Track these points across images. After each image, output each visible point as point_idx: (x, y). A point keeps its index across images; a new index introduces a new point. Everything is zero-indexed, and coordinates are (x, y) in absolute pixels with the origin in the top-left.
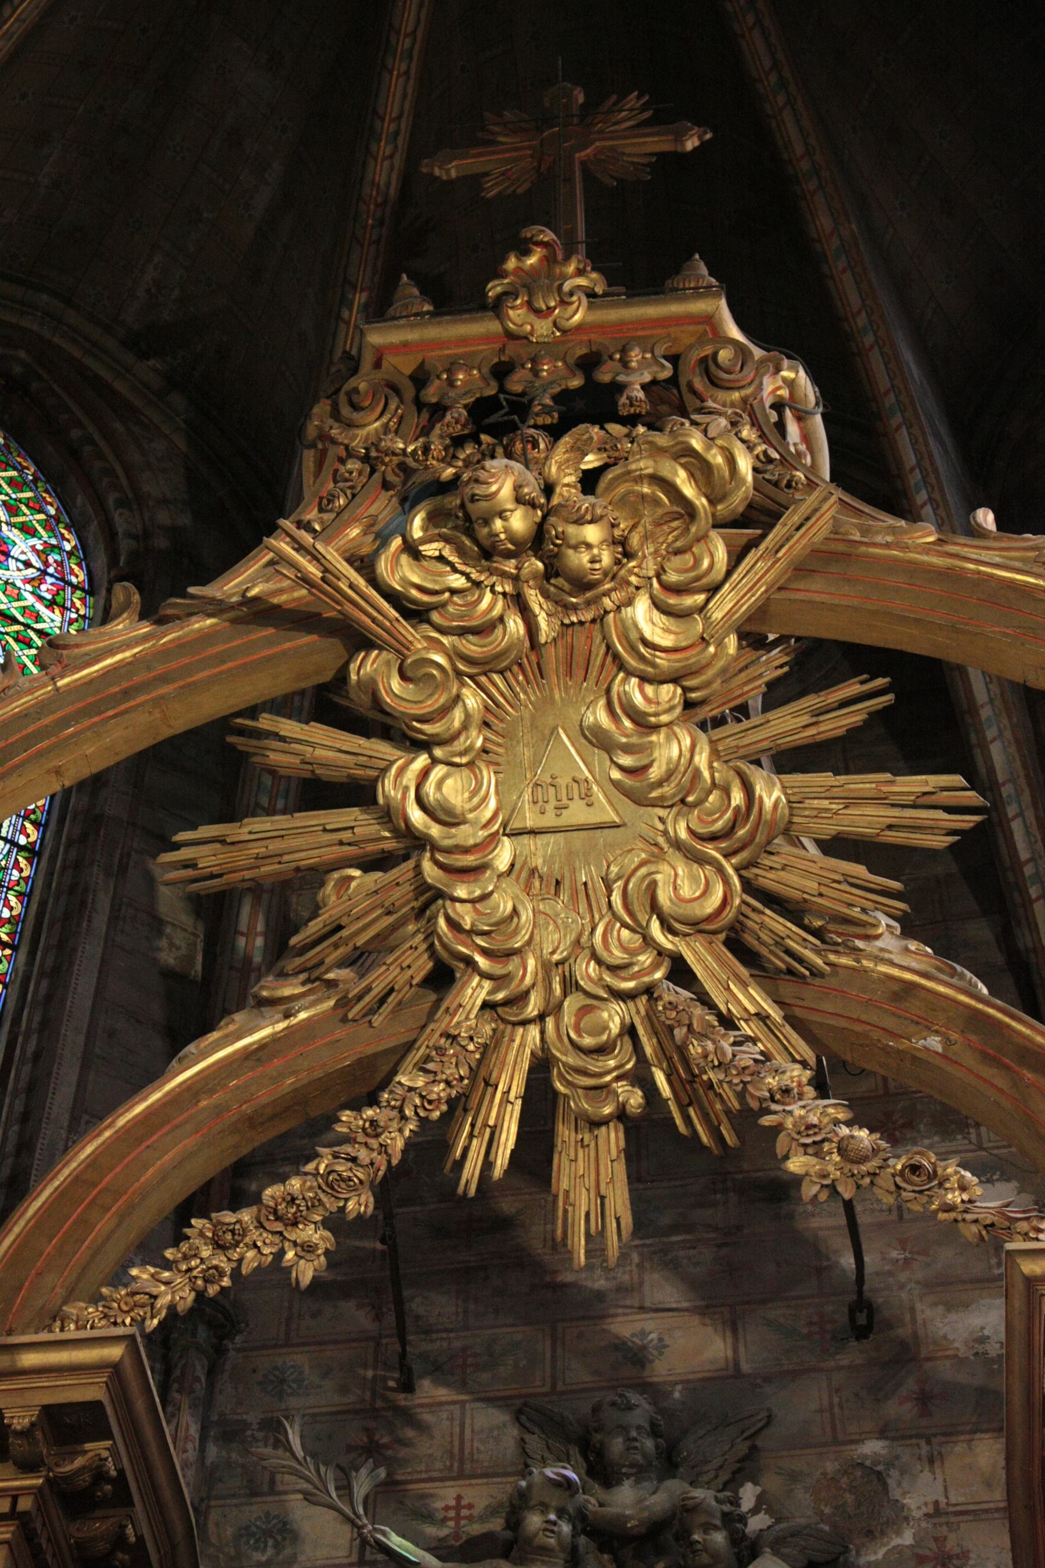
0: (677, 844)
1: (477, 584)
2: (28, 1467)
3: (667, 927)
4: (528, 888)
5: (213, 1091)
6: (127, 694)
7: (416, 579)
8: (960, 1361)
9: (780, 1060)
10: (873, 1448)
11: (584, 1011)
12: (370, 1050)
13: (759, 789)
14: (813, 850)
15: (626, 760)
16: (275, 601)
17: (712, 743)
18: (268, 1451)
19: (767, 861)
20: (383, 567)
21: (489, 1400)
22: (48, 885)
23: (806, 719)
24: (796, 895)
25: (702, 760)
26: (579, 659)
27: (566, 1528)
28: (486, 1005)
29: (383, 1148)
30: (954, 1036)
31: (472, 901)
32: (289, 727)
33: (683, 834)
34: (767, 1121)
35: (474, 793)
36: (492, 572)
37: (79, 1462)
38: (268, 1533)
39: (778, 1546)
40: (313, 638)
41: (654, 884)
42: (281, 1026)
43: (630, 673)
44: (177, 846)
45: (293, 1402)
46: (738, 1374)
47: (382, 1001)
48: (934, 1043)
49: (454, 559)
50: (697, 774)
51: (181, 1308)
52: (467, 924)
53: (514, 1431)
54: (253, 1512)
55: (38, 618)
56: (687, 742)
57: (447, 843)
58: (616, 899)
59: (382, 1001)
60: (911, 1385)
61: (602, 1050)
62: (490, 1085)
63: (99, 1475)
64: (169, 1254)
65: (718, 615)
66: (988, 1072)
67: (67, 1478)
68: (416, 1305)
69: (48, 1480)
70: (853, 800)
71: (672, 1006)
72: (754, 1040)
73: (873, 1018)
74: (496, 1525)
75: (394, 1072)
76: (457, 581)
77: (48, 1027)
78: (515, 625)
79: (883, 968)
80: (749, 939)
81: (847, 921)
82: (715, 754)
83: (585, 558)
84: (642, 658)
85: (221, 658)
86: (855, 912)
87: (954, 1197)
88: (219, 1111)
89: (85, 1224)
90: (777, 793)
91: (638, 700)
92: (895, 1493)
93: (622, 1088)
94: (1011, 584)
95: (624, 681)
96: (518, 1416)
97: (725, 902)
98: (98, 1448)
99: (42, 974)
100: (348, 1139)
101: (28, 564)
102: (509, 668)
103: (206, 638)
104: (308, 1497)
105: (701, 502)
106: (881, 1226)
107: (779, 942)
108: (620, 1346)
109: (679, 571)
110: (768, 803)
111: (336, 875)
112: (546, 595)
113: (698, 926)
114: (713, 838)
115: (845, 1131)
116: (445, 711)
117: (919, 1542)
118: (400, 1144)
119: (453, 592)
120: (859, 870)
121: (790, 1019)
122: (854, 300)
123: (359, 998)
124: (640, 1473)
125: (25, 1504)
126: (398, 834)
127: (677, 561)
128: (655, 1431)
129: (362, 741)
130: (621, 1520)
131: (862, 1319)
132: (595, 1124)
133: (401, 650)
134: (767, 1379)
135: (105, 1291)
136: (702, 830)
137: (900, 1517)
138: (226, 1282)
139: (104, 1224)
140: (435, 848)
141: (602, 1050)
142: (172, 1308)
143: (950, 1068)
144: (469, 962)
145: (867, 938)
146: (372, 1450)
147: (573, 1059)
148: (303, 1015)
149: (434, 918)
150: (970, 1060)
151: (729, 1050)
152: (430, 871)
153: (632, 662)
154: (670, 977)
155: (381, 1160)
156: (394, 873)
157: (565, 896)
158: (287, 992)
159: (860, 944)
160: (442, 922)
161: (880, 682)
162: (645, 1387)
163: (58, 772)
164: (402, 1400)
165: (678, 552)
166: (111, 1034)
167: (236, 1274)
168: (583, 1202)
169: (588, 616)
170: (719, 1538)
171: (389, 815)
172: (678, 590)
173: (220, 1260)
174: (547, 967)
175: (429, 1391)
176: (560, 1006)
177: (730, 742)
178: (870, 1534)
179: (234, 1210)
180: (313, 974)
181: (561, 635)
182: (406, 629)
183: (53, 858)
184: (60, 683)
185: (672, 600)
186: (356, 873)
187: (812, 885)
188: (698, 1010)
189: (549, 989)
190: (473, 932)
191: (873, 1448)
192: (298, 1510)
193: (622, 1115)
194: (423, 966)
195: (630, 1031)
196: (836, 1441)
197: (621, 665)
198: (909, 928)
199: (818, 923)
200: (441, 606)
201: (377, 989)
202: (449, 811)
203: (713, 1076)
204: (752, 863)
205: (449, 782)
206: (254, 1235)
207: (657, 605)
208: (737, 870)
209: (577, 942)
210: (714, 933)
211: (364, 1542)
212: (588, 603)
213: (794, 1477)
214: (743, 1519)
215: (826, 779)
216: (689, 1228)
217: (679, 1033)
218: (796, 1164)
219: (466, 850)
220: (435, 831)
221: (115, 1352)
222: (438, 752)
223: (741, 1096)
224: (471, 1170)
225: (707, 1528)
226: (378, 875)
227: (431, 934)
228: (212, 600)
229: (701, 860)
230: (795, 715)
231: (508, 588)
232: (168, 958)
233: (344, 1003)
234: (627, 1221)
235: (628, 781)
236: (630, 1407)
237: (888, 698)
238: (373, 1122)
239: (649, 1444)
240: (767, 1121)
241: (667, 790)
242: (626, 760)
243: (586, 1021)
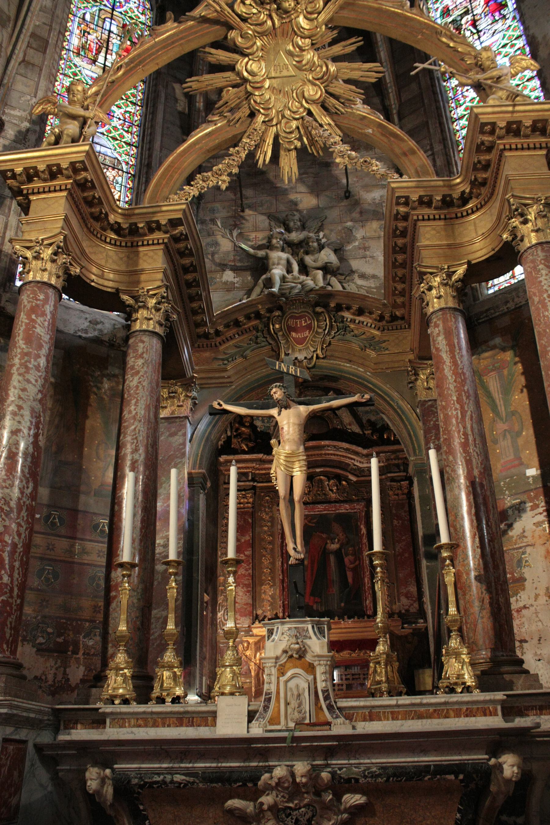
0: (309, 81)
1: (260, 12)
2: (166, 232)
3: (307, 102)
4: (273, 92)
5: (199, 144)
6: (173, 43)
7: (244, 10)
8: (369, 204)
9: (334, 135)
10: (349, 224)
11: (287, 123)
12: (236, 133)
13: (330, 67)
14: (341, 82)
15: (297, 59)
16: (208, 16)
17: (318, 54)
18: (212, 226)
19: (331, 85)
20: (236, 7)
21: (262, 214)
22: (149, 90)
23: (341, 48)
24: (338, 94)
25: (316, 59)
26: (285, 32)
27: (281, 242)
28: (263, 122)
29: (240, 157)
30: (375, 129)
31: (260, 96)
32: (213, 51)
33: (311, 78)
34: (331, 150)
35: (260, 68)
36: (263, 8)
37: (177, 231)
38: (213, 244)
39: (328, 245)
40: (218, 27)
41: (303, 92)
42: (214, 127)
43: (298, 36)
44: (187, 82)
45: (217, 215)
46: (319, 207)
47: (238, 121)
48: (370, 131)
49: (254, 5)
50: (314, 63)
51: (196, 196)
52: (258, 101)
53: (268, 221)
54: (209, 240)
55: (139, 18)
56: (312, 54)
57: (253, 81)
58: (294, 95)
59: (238, 121)
60: (358, 210)
61: (291, 133)
62: (265, 141)
63: (182, 234)
64: (192, 183)
65: (320, 20)
66: (383, 138)
67: (175, 235)
68: (244, 192)
70: (352, 70)
71: (308, 122)
72: (327, 130)
73: (356, 124)
74: (264, 242)
75: (241, 138)
76: (255, 11)
77: (152, 127)
78: (269, 23)
79: (358, 112)
80: (326, 105)
81: (350, 100)
82: (319, 57)
83: (287, 4)
84: (301, 32)
85: (196, 32)
86: (352, 98)
87: (375, 168)
88: (201, 148)
89: (172, 176)
90: (334, 68)
91: (300, 43)
92: (354, 234)
93: (296, 141)
94: (394, 12)
96: (268, 217)
97: (321, 96)
98: (181, 228)
99: (150, 113)
100: (231, 155)
101: (135, 3)
103: (191, 27)
104: (223, 237)
106: (352, 173)
107: (334, 105)
108: (291, 201)
109: (311, 8)
110: (332, 70)
111: (226, 89)
112: (277, 15)
113: (314, 102)
114: (318, 79)
115: (349, 152)
116: (252, 46)
117: (360, 244)
118: (244, 156)
119: (254, 14)
120: (353, 88)
121: (336, 125)
123: (233, 120)
124: (297, 230)
125: (166, 241)
126: (241, 79)
127: (310, 5)
128: (300, 221)
129: (231, 54)
130: (293, 241)
131: (347, 195)
132: (289, 150)
133: (241, 30)
134: (326, 208)
135: (178, 192)
136: (316, 77)
137: (356, 239)
138: (206, 189)
139: (176, 176)
140: (250, 82)
141: (291, 133)
142: (194, 196)
143: (374, 137)
144: (259, 111)
145: (355, 104)
146: (235, 226)
147: (284, 135)
148: (219, 125)
149: (250, 100)
150: (378, 135)
151: (322, 133)
152: (249, 88)
153: (299, 33)
154: (308, 114)
155: (240, 160)
156: (240, 88)
157: (282, 94)
158: (215, 119)
159: (353, 106)
160: (252, 101)
161: (360, 38)
162: (297, 211)
163: (157, 64)
164: (241, 214)
165: (311, 3)
166: (168, 128)
167: (208, 188)
168: (287, 169)
169: (288, 20)
170: (315, 244)
171: (239, 74)
173: (204, 184)
174: (278, 112)
175: (248, 212)
176: (281, 122)
177: (323, 54)
178: (348, 243)
179: (207, 172)
180: (221, 114)
181: (281, 26)
182: (242, 24)
183: (149, 83)
184: (157, 40)
185: (309, 16)
186: (231, 89)
187: (342, 91)
188: (314, 123)
189: (278, 118)
190: (260, 103)
191: (349, 224)
192: (220, 239)
193: (296, 148)
194: (248, 112)
195: (298, 128)
196: (341, 222)
197: (296, 34)
198: (365, 102)
199: (343, 101)
200: (251, 18)
201: (237, 118)
202: (254, 73)
203: (317, 138)
204: (327, 86)
205: (253, 65)
206: (212, 178)
207: (305, 17)
208: (324, 87)
209: (285, 106)
211: (235, 245)
212: (288, 17)
213: (331, 231)
214: (321, 240)
215: (346, 64)
216: (307, 173)
217: (310, 128)
218: (338, 160)
219: (258, 83)
220: (250, 78)
221: (184, 207)
222: (250, 57)
223: (324, 144)
224: (261, 162)
225: (313, 242)
226: (236, 89)
227: (249, 104)
228: (192, 17)
229: (315, 85)
230: (339, 47)
231: (268, 13)
232: (180, 109)
233: (229, 121)
234: (297, 173)
235: (298, 65)
236: (294, 215)
237: (362, 43)
238: (238, 151)
239: (299, 223)
240: (331, 150)
241: (307, 67)
242: (297, 59)
243: (288, 125)
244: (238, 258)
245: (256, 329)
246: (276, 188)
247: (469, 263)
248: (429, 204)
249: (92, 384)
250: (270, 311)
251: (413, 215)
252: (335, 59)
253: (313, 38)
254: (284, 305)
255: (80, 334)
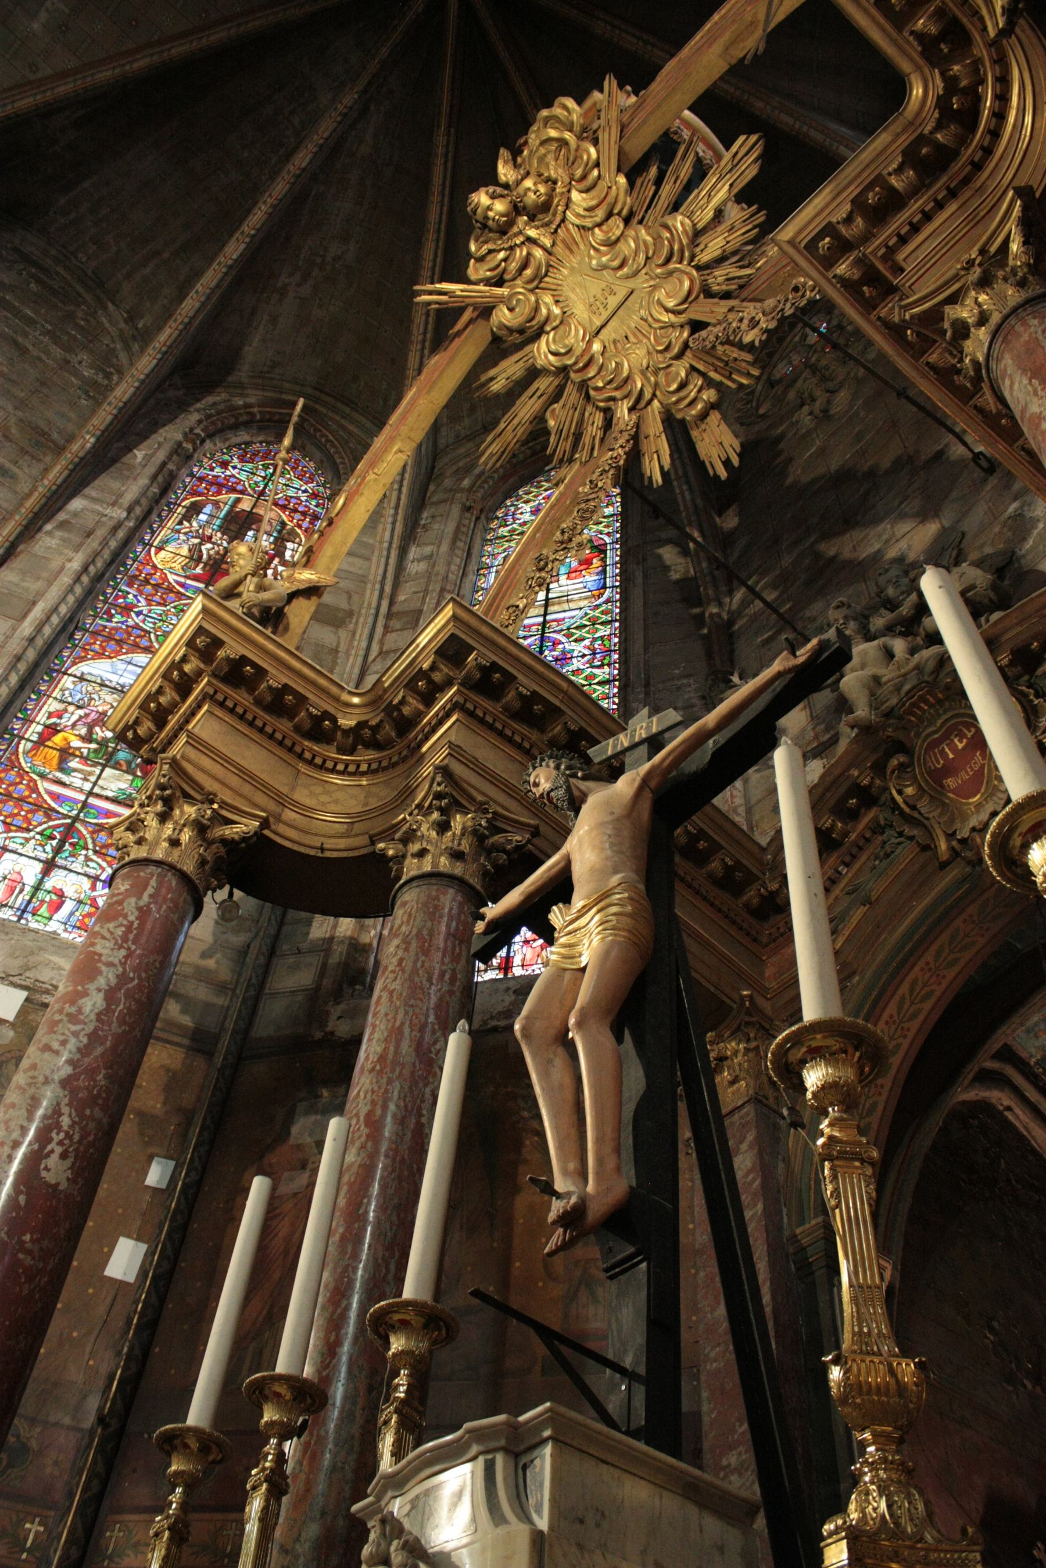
69: (460, 684)
95: (593, 234)
97: (692, 281)
102: (547, 271)
105: (567, 135)
119: (505, 260)
122: (790, 120)
144: (613, 399)
172: (584, 177)
204: (692, 258)
210: (697, 297)
229: (670, 274)
244: (822, 726)
245: (877, 829)
246: (860, 563)
247: (1023, 192)
248: (894, 201)
249: (526, 1114)
250: (879, 768)
251: (874, 253)
252: (675, 207)
253: (616, 211)
254: (900, 736)
255: (494, 1023)
